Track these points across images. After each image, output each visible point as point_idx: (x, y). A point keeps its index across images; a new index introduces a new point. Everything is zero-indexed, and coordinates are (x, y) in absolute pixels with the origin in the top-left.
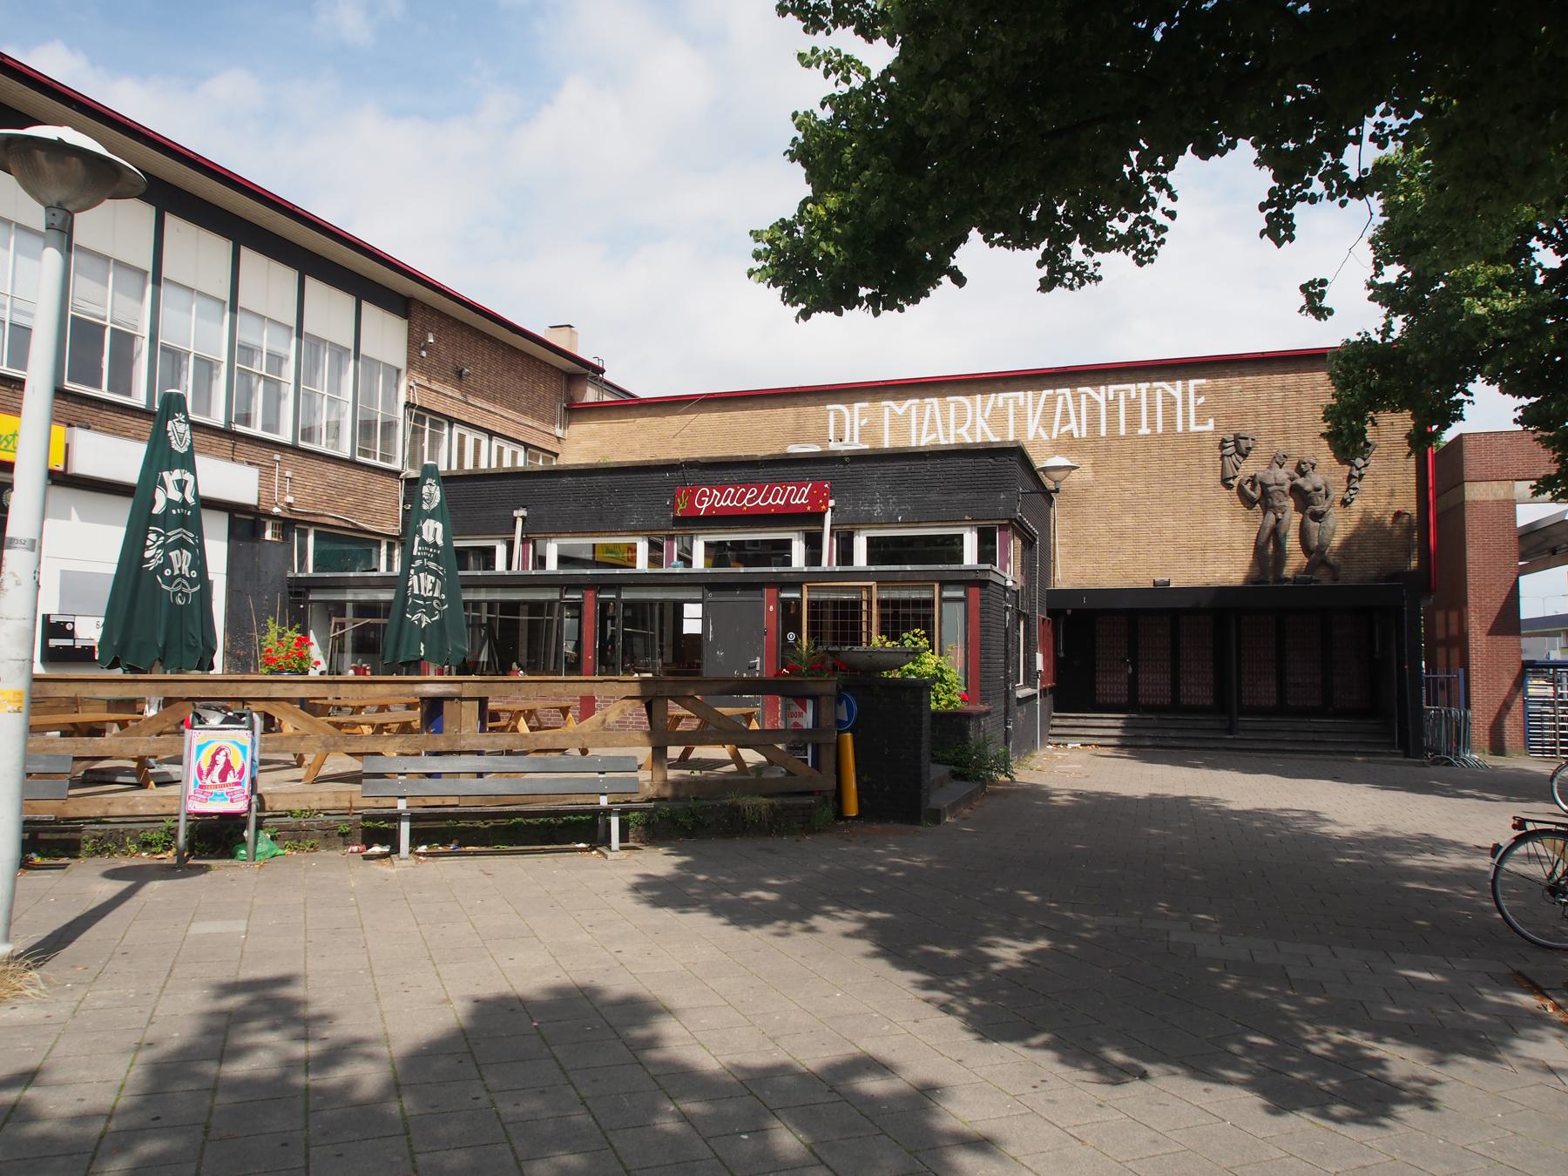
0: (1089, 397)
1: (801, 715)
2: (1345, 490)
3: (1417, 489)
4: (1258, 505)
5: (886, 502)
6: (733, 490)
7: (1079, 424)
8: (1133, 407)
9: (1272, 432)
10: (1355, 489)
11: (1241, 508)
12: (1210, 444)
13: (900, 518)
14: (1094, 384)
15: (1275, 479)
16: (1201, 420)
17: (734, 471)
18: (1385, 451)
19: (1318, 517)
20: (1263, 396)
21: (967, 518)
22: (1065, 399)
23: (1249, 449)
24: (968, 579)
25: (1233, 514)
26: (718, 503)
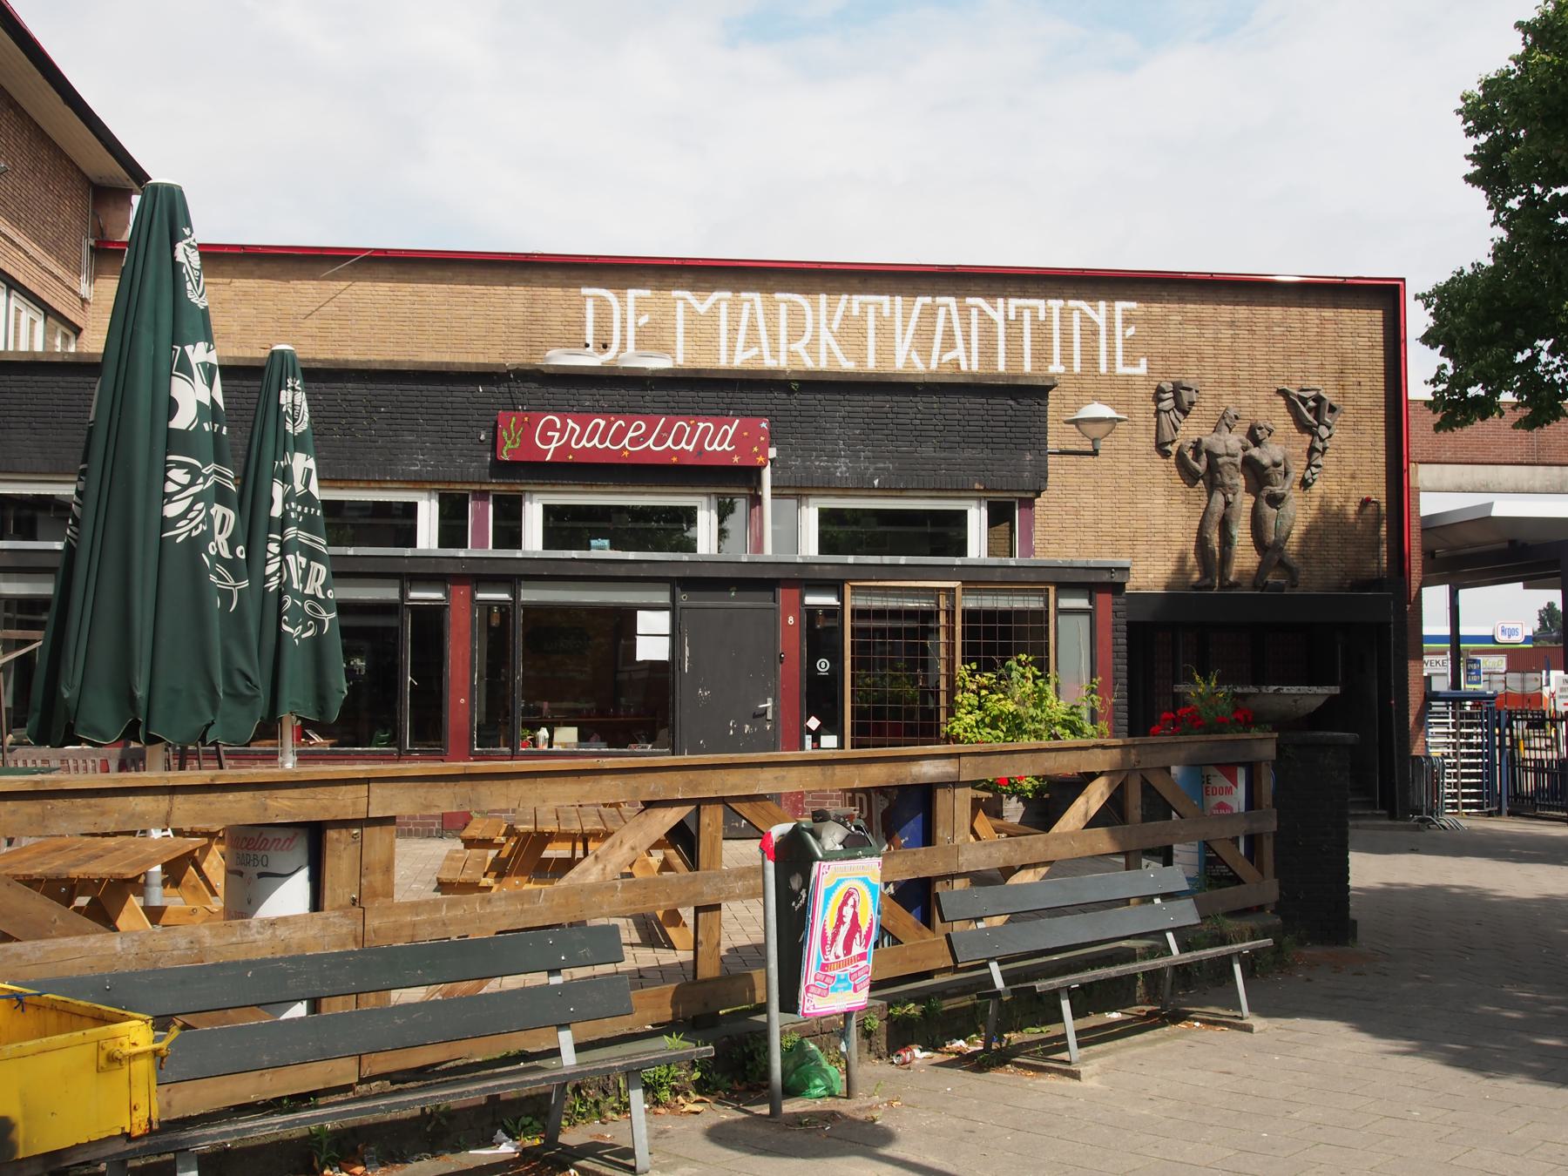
0: (981, 312)
1: (1229, 791)
2: (1305, 467)
3: (1386, 471)
4: (1201, 482)
5: (855, 456)
6: (603, 423)
7: (968, 350)
8: (1042, 332)
9: (1219, 383)
10: (1318, 466)
11: (1180, 485)
12: (1141, 393)
13: (876, 482)
14: (989, 295)
15: (1226, 446)
16: (1130, 360)
17: (602, 392)
18: (1350, 418)
19: (1276, 501)
20: (1209, 333)
21: (977, 486)
22: (949, 313)
23: (1192, 403)
24: (1099, 580)
25: (1170, 492)
26: (577, 444)
